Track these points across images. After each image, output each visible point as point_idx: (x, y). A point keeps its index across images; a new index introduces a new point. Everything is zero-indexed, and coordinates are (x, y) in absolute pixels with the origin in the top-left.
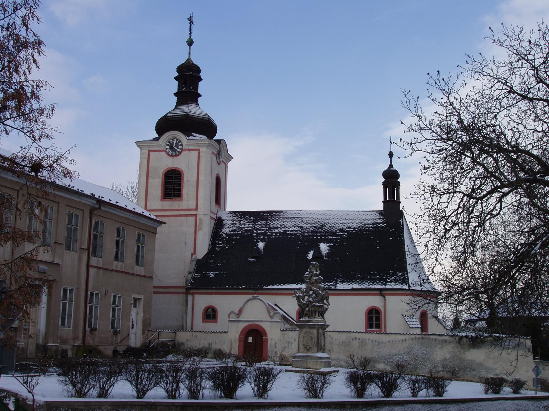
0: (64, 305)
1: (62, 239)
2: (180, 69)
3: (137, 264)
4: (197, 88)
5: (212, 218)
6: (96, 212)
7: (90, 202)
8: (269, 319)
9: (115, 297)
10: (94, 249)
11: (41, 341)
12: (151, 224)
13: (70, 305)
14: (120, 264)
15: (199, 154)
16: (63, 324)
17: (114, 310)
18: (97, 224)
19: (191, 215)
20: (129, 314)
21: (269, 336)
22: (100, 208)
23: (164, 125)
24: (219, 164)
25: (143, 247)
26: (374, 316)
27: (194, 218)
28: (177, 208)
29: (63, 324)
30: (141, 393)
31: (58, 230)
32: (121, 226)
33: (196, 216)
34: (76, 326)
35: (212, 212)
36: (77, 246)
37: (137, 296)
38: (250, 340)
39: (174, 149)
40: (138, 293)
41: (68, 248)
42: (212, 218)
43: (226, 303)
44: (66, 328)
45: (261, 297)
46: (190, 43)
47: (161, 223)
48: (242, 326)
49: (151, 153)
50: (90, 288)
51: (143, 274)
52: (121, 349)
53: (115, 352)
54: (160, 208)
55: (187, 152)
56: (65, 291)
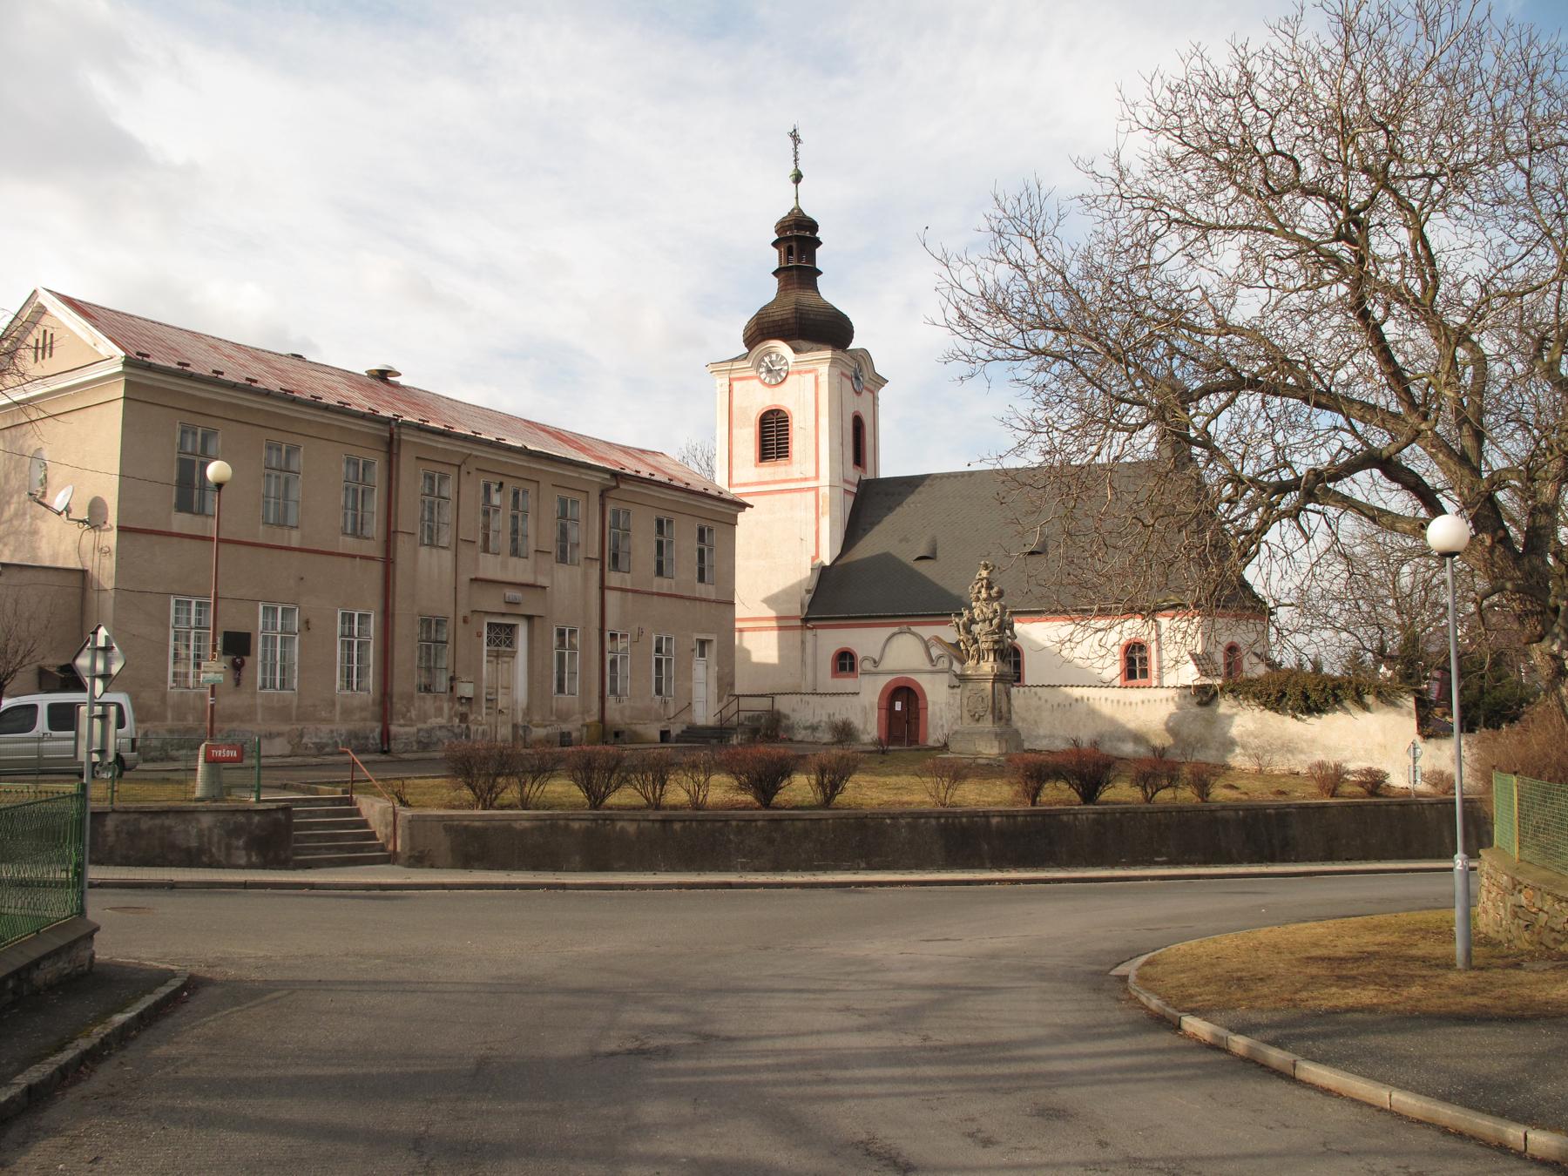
0: (561, 657)
1: (550, 542)
2: (782, 227)
3: (701, 579)
4: (812, 258)
5: (846, 491)
6: (613, 494)
7: (598, 478)
8: (928, 667)
9: (659, 641)
10: (613, 558)
11: (520, 719)
12: (722, 507)
13: (573, 656)
14: (665, 582)
15: (816, 378)
16: (561, 689)
17: (659, 662)
18: (616, 514)
19: (809, 489)
20: (689, 668)
21: (929, 698)
22: (617, 487)
23: (761, 330)
24: (858, 393)
25: (711, 550)
26: (1137, 656)
27: (811, 495)
28: (784, 477)
29: (561, 689)
30: (596, 799)
31: (540, 530)
32: (664, 515)
33: (816, 489)
34: (585, 692)
35: (846, 481)
36: (580, 554)
37: (703, 637)
38: (898, 706)
39: (776, 376)
40: (703, 631)
41: (562, 558)
42: (846, 491)
43: (864, 640)
44: (566, 697)
45: (914, 629)
46: (798, 178)
47: (743, 506)
48: (883, 681)
49: (735, 384)
50: (610, 625)
51: (713, 597)
52: (675, 730)
53: (665, 735)
54: (755, 479)
55: (797, 376)
56: (561, 633)
